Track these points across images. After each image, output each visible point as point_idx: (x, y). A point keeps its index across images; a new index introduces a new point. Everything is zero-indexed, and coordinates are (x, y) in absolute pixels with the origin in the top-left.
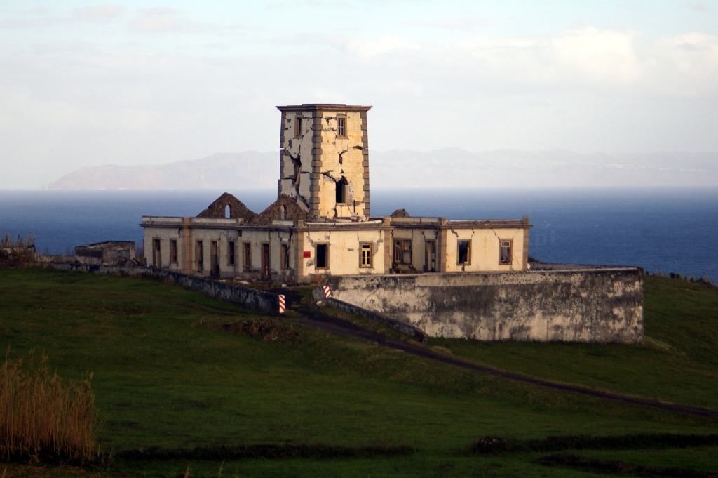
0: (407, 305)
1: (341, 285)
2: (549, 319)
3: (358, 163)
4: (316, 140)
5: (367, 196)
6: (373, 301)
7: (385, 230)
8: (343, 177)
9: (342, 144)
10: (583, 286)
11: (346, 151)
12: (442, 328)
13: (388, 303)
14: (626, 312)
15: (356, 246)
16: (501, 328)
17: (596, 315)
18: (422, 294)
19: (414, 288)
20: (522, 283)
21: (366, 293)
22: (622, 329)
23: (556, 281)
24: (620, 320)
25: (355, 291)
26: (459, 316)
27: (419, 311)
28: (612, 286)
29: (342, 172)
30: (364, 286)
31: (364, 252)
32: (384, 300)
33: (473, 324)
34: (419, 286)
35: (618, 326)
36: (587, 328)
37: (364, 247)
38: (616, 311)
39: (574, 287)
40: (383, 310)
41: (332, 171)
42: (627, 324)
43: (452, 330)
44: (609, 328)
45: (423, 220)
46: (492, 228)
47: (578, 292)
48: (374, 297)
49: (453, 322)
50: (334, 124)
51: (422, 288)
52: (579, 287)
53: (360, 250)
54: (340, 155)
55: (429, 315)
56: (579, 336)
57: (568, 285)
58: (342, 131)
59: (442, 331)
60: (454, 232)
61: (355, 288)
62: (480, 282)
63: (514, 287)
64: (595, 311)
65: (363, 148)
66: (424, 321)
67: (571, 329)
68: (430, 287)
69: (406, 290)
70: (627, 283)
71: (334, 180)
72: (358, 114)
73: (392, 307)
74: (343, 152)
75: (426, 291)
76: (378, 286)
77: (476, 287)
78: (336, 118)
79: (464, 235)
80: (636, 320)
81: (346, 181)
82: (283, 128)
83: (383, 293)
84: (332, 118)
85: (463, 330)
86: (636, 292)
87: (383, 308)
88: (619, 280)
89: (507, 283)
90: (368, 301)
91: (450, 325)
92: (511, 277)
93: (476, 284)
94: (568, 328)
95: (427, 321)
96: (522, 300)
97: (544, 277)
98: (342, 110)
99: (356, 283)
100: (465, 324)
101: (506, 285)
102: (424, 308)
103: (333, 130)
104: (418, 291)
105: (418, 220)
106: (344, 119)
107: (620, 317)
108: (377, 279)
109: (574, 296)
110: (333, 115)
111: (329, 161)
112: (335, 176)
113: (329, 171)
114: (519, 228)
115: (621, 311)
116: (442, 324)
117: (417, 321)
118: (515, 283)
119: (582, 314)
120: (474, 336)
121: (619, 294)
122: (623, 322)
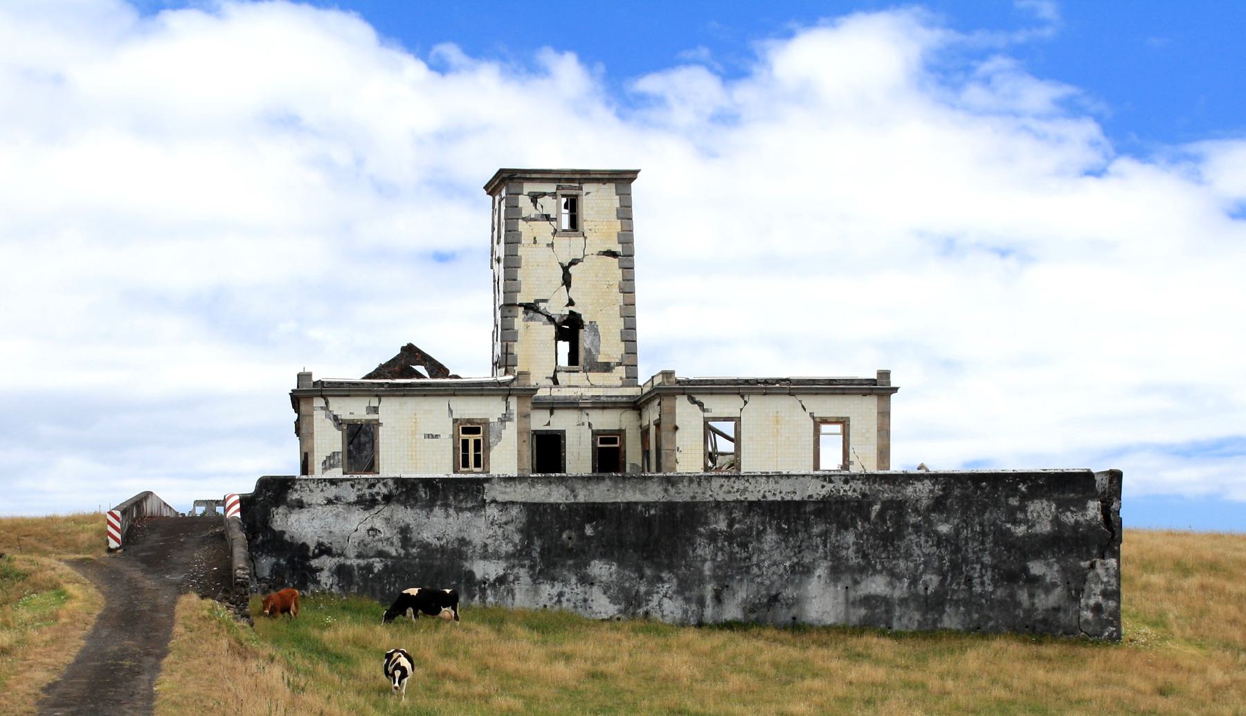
0: (463, 542)
2: (849, 582)
3: (609, 286)
5: (631, 351)
7: (519, 397)
8: (571, 312)
9: (569, 248)
10: (939, 505)
12: (561, 594)
13: (415, 536)
14: (1064, 570)
15: (446, 429)
16: (718, 598)
17: (981, 576)
18: (504, 519)
19: (483, 504)
20: (770, 498)
22: (1056, 610)
23: (864, 495)
24: (1048, 589)
25: (329, 508)
26: (599, 569)
27: (496, 556)
28: (1022, 508)
29: (571, 303)
30: (352, 497)
31: (465, 443)
32: (405, 531)
33: (643, 589)
34: (494, 501)
36: (957, 604)
37: (465, 431)
38: (1036, 568)
39: (916, 511)
40: (402, 552)
41: (545, 301)
42: (1070, 596)
43: (585, 600)
44: (1018, 605)
48: (378, 524)
51: (504, 506)
52: (930, 509)
53: (455, 437)
54: (566, 269)
55: (523, 566)
56: (243, 569)
57: (898, 507)
59: (559, 601)
60: (694, 402)
61: (330, 502)
64: (978, 567)
65: (623, 255)
66: (511, 578)
67: (912, 605)
68: (524, 504)
69: (459, 510)
70: (1063, 505)
71: (551, 319)
72: (611, 188)
73: (426, 546)
74: (571, 264)
75: (514, 511)
76: (388, 499)
77: (647, 505)
78: (554, 195)
79: (719, 406)
80: (1098, 589)
83: (405, 515)
84: (544, 194)
85: (614, 600)
86: (1090, 526)
87: (402, 547)
88: (1041, 497)
89: (730, 498)
90: (362, 531)
91: (580, 589)
92: (739, 485)
93: (651, 498)
94: (903, 602)
95: (517, 578)
97: (829, 487)
98: (571, 184)
99: (332, 492)
100: (622, 589)
102: (510, 548)
104: (492, 511)
106: (577, 196)
107: (1048, 580)
108: (385, 485)
109: (917, 528)
110: (551, 188)
111: (539, 281)
112: (552, 312)
113: (537, 301)
115: (1049, 566)
116: (558, 587)
117: (492, 577)
118: (752, 497)
119: (940, 572)
121: (1045, 527)
122: (1058, 591)
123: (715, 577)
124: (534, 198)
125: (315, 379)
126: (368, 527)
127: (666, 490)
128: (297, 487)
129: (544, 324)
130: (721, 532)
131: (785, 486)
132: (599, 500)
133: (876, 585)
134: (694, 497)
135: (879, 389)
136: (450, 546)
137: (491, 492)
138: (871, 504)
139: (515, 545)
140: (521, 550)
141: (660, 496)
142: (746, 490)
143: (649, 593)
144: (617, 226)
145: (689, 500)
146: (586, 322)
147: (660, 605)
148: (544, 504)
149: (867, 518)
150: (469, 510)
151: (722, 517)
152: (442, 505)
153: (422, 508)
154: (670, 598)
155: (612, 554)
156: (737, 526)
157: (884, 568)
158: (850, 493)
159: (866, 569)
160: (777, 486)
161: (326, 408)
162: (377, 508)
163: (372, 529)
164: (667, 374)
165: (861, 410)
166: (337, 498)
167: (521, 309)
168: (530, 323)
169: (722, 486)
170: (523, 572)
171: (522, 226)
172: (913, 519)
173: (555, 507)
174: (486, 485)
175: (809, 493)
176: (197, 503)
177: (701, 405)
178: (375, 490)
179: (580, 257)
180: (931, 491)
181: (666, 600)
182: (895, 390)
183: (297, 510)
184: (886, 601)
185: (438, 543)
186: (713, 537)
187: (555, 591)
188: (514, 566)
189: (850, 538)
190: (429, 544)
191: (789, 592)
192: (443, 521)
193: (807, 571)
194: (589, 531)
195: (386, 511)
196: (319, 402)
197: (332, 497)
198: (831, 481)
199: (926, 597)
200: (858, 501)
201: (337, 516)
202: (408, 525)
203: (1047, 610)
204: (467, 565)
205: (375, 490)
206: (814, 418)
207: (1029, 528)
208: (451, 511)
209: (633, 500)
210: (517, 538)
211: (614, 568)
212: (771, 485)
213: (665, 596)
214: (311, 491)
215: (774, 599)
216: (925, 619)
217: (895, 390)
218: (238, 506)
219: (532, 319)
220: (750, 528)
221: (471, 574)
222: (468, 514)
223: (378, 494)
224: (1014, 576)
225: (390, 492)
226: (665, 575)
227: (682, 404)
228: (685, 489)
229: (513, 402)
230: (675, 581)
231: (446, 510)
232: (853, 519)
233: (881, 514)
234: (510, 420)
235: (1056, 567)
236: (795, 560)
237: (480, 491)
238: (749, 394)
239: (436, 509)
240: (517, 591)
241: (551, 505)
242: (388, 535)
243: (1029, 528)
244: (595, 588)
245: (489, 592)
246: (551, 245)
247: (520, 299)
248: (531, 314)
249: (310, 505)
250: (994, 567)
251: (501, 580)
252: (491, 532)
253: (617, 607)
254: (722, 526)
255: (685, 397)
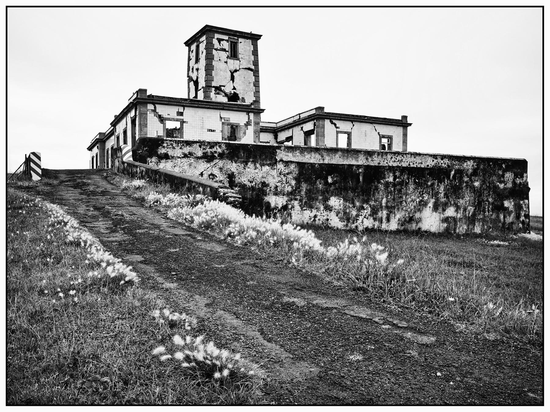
0: (264, 184)
1: (162, 151)
4: (210, 58)
6: (212, 176)
7: (254, 113)
9: (233, 64)
10: (475, 172)
11: (238, 70)
12: (315, 216)
13: (237, 180)
14: (515, 205)
16: (388, 220)
17: (488, 208)
18: (287, 172)
20: (412, 166)
21: (203, 166)
22: (512, 223)
23: (448, 166)
25: (184, 160)
26: (335, 202)
28: (503, 176)
29: (234, 88)
30: (200, 153)
32: (231, 176)
34: (281, 160)
35: (510, 219)
36: (479, 220)
38: (506, 204)
39: (467, 175)
41: (224, 86)
44: (500, 221)
45: (302, 116)
46: (371, 123)
47: (471, 180)
48: (216, 172)
49: (328, 208)
50: (226, 45)
51: (287, 163)
54: (232, 73)
55: (296, 200)
57: (460, 173)
58: (234, 54)
59: (314, 220)
60: (332, 123)
61: (185, 156)
62: (361, 161)
63: (403, 170)
64: (487, 203)
66: (290, 206)
69: (262, 165)
72: (249, 42)
74: (236, 71)
75: (292, 167)
76: (221, 156)
77: (359, 167)
78: (227, 41)
81: (239, 97)
82: (189, 59)
83: (233, 167)
84: (223, 40)
85: (341, 219)
89: (395, 164)
91: (325, 213)
93: (360, 163)
94: (460, 219)
95: (293, 207)
96: (412, 187)
97: (435, 161)
98: (235, 35)
101: (393, 167)
102: (289, 189)
103: (224, 50)
104: (280, 166)
105: (298, 117)
108: (220, 147)
110: (226, 38)
113: (221, 86)
114: (398, 126)
115: (510, 202)
116: (314, 212)
117: (280, 206)
118: (404, 165)
120: (357, 227)
123: (387, 207)
124: (220, 40)
125: (148, 94)
126: (209, 173)
127: (367, 159)
128: (165, 145)
129: (223, 96)
130: (391, 183)
131: (418, 159)
132: (334, 163)
133: (451, 212)
134: (379, 163)
135: (403, 123)
136: (257, 187)
137: (281, 155)
138: (451, 171)
139: (292, 187)
140: (296, 190)
141: (364, 162)
142: (402, 160)
143: (357, 216)
144: (252, 58)
145: (377, 165)
146: (241, 98)
147: (362, 222)
148: (308, 163)
149: (449, 178)
150: (268, 165)
151: (391, 175)
152: (253, 161)
153: (241, 162)
154: (367, 218)
155: (341, 194)
156: (397, 180)
157: (455, 203)
158: (443, 165)
159: (445, 206)
160: (415, 159)
161: (154, 111)
162: (216, 161)
163: (212, 174)
164: (322, 108)
165: (396, 132)
166: (191, 154)
167: (213, 89)
168: (217, 95)
169: (392, 158)
170: (296, 203)
171: (214, 52)
172: (466, 179)
173: (312, 165)
174: (278, 151)
175: (427, 164)
176: (90, 149)
177: (335, 125)
178: (214, 150)
179: (238, 69)
180: (473, 166)
181: (365, 219)
182: (410, 124)
183: (164, 161)
184: (454, 219)
185: (250, 185)
186: (387, 184)
187: (312, 215)
188: (291, 200)
189: (442, 188)
190: (245, 185)
191: (417, 215)
192: (253, 171)
193: (426, 204)
194: (330, 180)
195: (221, 163)
196: (150, 107)
197: (187, 152)
198: (436, 159)
199: (469, 217)
200: (446, 169)
201: (190, 165)
202: (233, 173)
203: (509, 223)
204: (267, 199)
205: (214, 150)
206: (379, 135)
207: (505, 185)
208: (258, 165)
209: (352, 164)
210: (293, 183)
211: (342, 201)
212: (413, 159)
213: (365, 217)
214: (174, 148)
215: (411, 219)
216: (468, 228)
217: (410, 124)
218: (131, 153)
219: (218, 94)
220: (403, 181)
221: (268, 204)
222: (267, 167)
223: (216, 152)
224: (499, 208)
225: (223, 151)
226: (365, 206)
227: (327, 122)
228: (375, 159)
229: (252, 115)
230: (369, 209)
231: (255, 165)
232: (444, 178)
233: (454, 176)
234: (250, 125)
235: (513, 204)
236: (421, 198)
237: (275, 154)
238: (355, 121)
239: (249, 163)
240: (293, 215)
241: (311, 164)
242: (221, 179)
243: (505, 185)
244: (332, 213)
245: (278, 215)
246: (226, 62)
247: (214, 84)
248: (218, 91)
249: (173, 157)
250: (493, 203)
251: (285, 208)
252: (280, 179)
253: (343, 223)
254: (391, 179)
255: (329, 120)
